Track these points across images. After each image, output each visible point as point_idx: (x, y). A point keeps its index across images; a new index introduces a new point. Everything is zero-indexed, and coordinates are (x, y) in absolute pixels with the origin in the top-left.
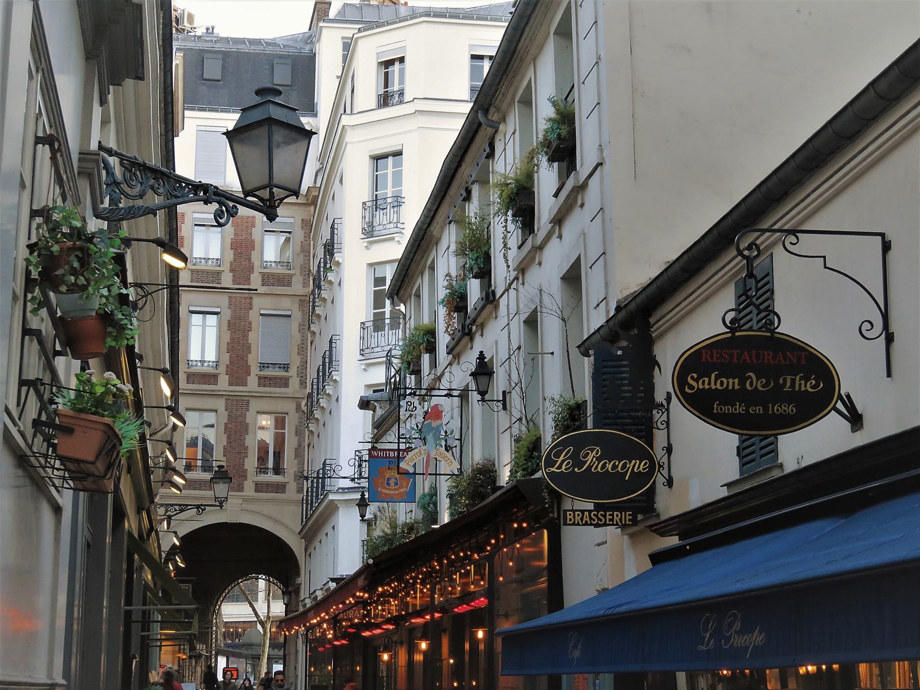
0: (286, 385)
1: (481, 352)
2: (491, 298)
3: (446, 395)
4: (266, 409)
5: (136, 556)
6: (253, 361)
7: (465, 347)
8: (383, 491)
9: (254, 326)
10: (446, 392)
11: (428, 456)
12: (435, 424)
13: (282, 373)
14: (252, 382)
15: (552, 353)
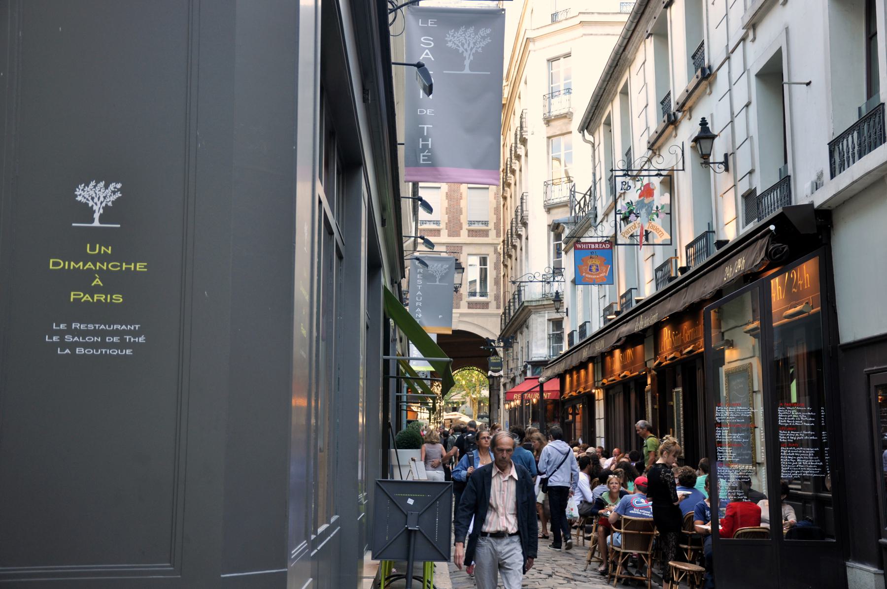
0: (487, 236)
1: (703, 119)
2: (708, 72)
3: (657, 175)
4: (474, 252)
5: (391, 321)
6: (464, 219)
7: (670, 136)
8: (588, 276)
9: (464, 196)
10: (656, 172)
11: (642, 228)
12: (646, 201)
13: (484, 227)
14: (464, 232)
15: (808, 84)
